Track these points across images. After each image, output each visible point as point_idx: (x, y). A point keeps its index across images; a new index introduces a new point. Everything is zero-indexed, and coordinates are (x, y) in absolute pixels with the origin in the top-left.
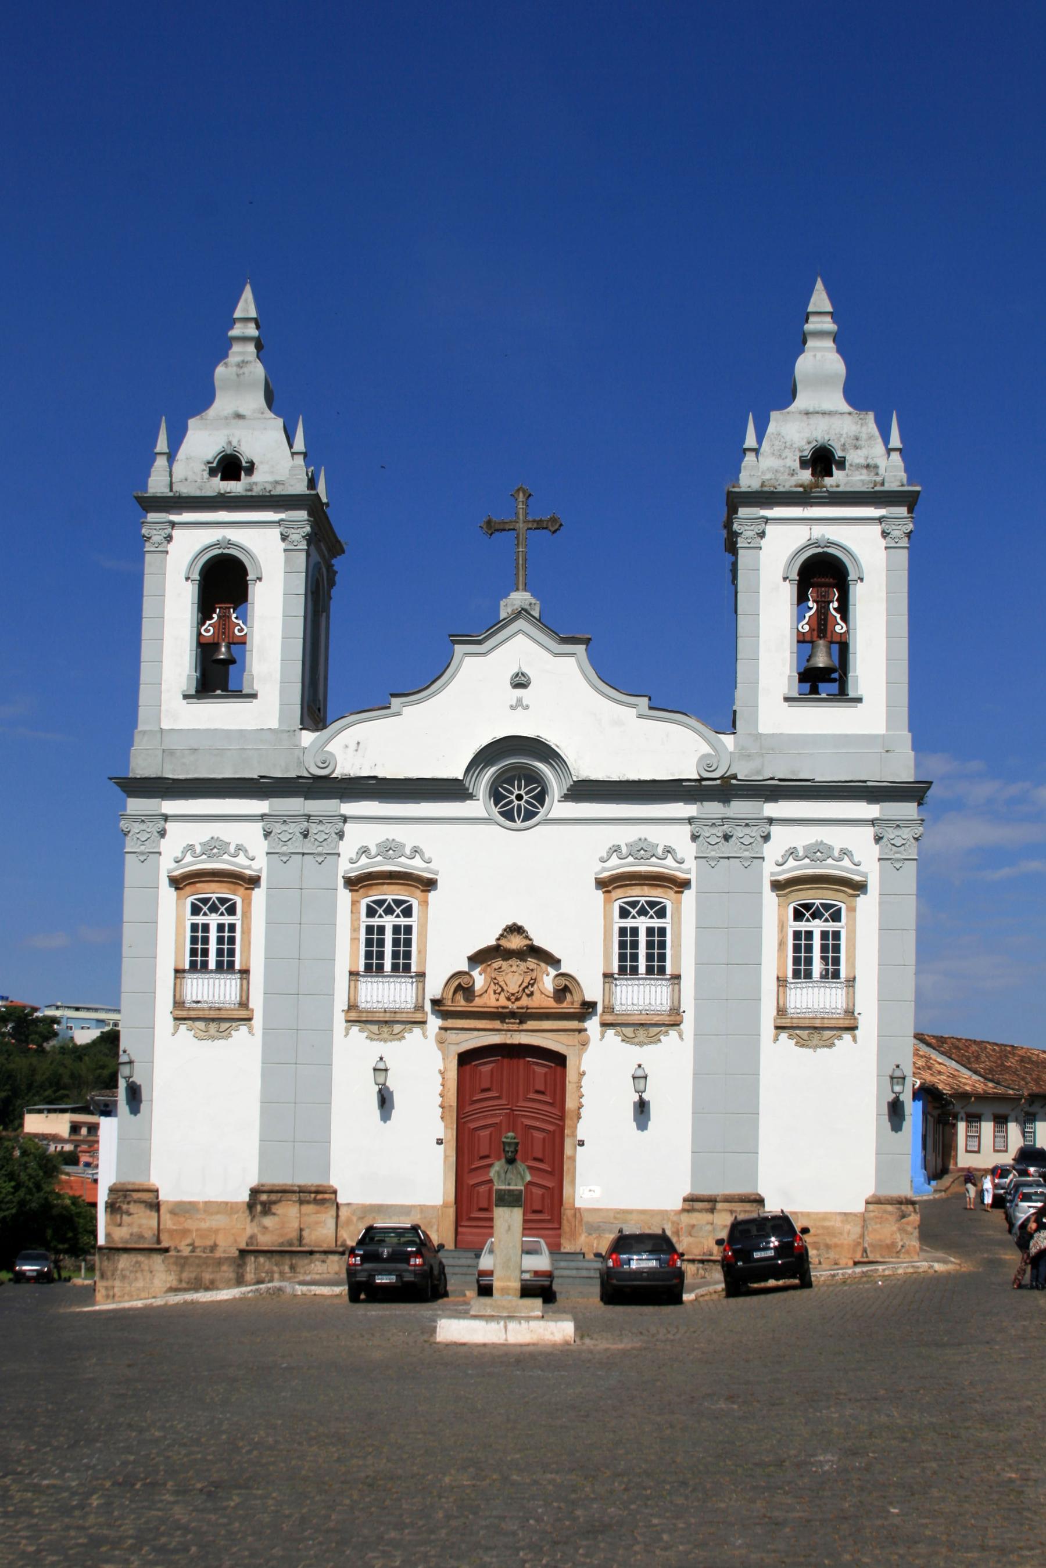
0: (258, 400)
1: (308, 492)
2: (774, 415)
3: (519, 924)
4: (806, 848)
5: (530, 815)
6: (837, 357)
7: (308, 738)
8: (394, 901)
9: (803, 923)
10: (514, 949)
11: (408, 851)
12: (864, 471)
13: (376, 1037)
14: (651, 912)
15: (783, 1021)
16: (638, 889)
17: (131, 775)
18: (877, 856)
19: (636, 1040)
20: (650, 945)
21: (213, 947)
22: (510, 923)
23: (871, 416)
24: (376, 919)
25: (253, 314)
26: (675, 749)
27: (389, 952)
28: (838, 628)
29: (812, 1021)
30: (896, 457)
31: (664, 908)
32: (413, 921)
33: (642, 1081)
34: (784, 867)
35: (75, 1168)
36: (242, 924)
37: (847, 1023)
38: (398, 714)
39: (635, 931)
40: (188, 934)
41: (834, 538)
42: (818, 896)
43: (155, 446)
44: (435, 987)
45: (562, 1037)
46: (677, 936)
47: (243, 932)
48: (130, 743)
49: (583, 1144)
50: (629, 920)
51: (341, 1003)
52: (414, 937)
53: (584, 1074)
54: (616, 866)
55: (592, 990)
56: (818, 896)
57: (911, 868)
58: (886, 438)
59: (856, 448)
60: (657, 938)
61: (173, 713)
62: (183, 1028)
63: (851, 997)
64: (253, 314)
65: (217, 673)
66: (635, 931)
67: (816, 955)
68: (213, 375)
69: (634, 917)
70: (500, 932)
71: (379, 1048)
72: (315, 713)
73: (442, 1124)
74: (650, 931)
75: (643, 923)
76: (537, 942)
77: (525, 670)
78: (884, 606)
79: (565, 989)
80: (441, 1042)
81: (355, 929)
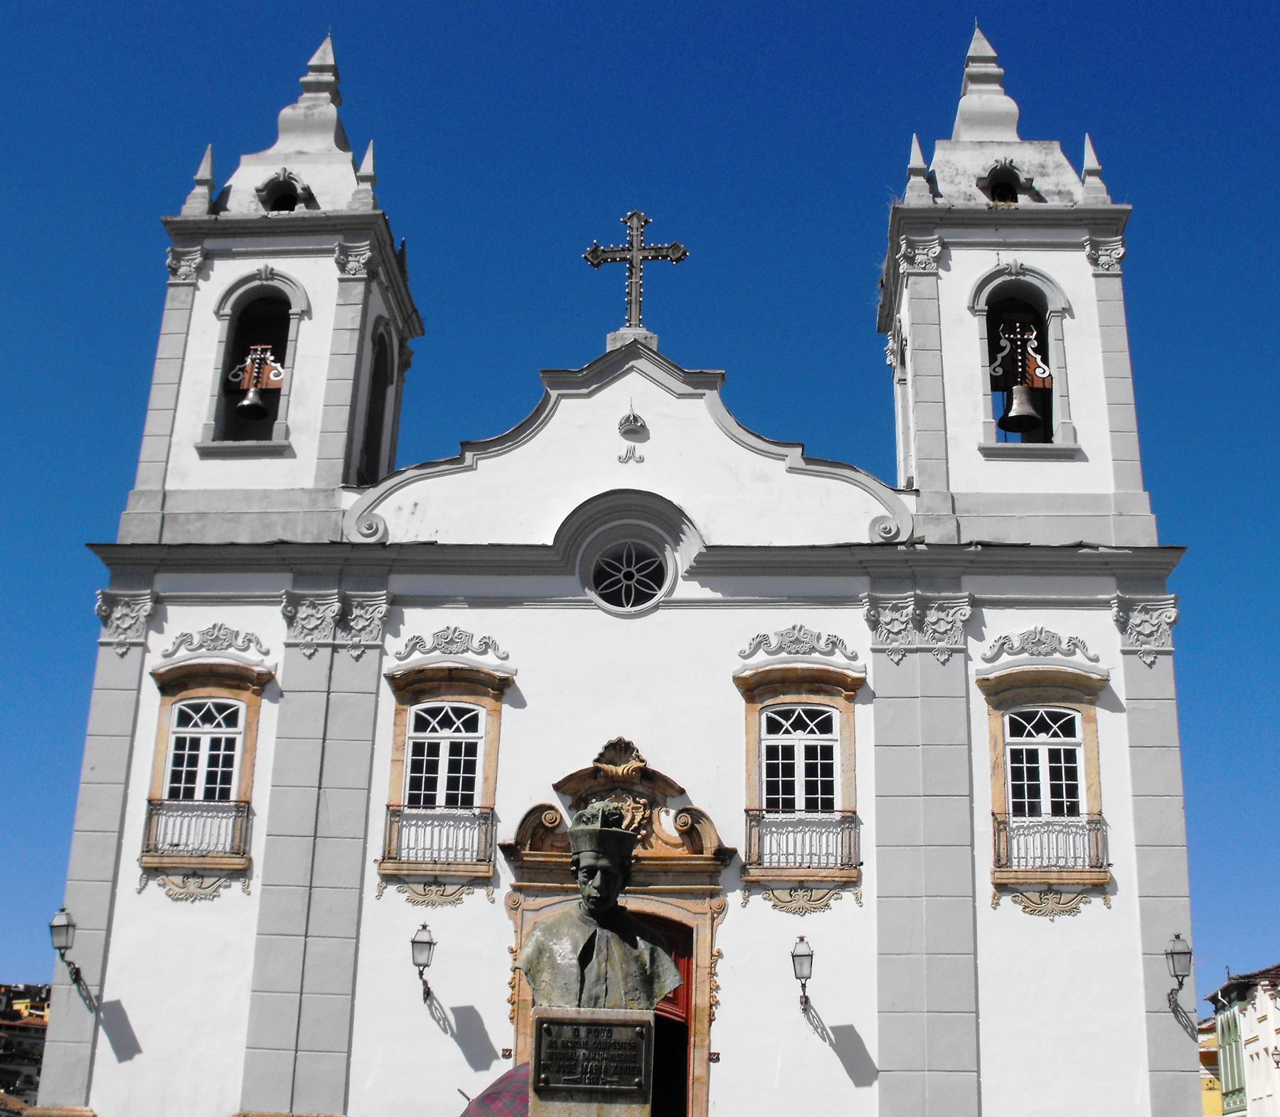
0: (327, 141)
1: (372, 212)
2: (939, 144)
3: (627, 739)
4: (1025, 638)
5: (642, 598)
6: (1007, 99)
7: (350, 500)
8: (453, 709)
9: (1024, 739)
10: (619, 777)
11: (475, 644)
12: (1056, 198)
13: (421, 899)
14: (812, 725)
15: (1005, 875)
16: (789, 694)
17: (118, 542)
18: (1120, 647)
19: (794, 905)
20: (810, 770)
21: (202, 769)
22: (614, 738)
23: (1056, 145)
24: (427, 734)
25: (330, 61)
26: (837, 510)
27: (441, 779)
28: (1038, 371)
29: (1045, 875)
30: (1094, 181)
31: (236, 713)
32: (238, 733)
33: (806, 961)
34: (997, 663)
35: (113, 1056)
36: (245, 739)
37: (1095, 877)
38: (471, 468)
39: (789, 751)
40: (171, 751)
41: (1027, 264)
42: (1039, 700)
43: (195, 173)
44: (507, 831)
45: (688, 903)
46: (851, 757)
47: (245, 751)
48: (123, 505)
49: (718, 1060)
50: (780, 735)
51: (375, 850)
52: (480, 759)
53: (720, 955)
54: (761, 660)
55: (729, 829)
56: (1039, 700)
57: (1166, 663)
58: (1076, 160)
59: (1043, 175)
60: (821, 759)
61: (185, 475)
62: (153, 884)
63: (1101, 844)
64: (330, 61)
65: (247, 420)
66: (789, 751)
67: (1036, 785)
68: (278, 112)
69: (787, 732)
70: (601, 750)
71: (424, 914)
72: (367, 466)
73: (512, 1028)
74: (810, 751)
75: (799, 740)
76: (653, 765)
77: (637, 413)
78: (1098, 341)
79: (693, 826)
80: (514, 907)
81: (399, 748)
